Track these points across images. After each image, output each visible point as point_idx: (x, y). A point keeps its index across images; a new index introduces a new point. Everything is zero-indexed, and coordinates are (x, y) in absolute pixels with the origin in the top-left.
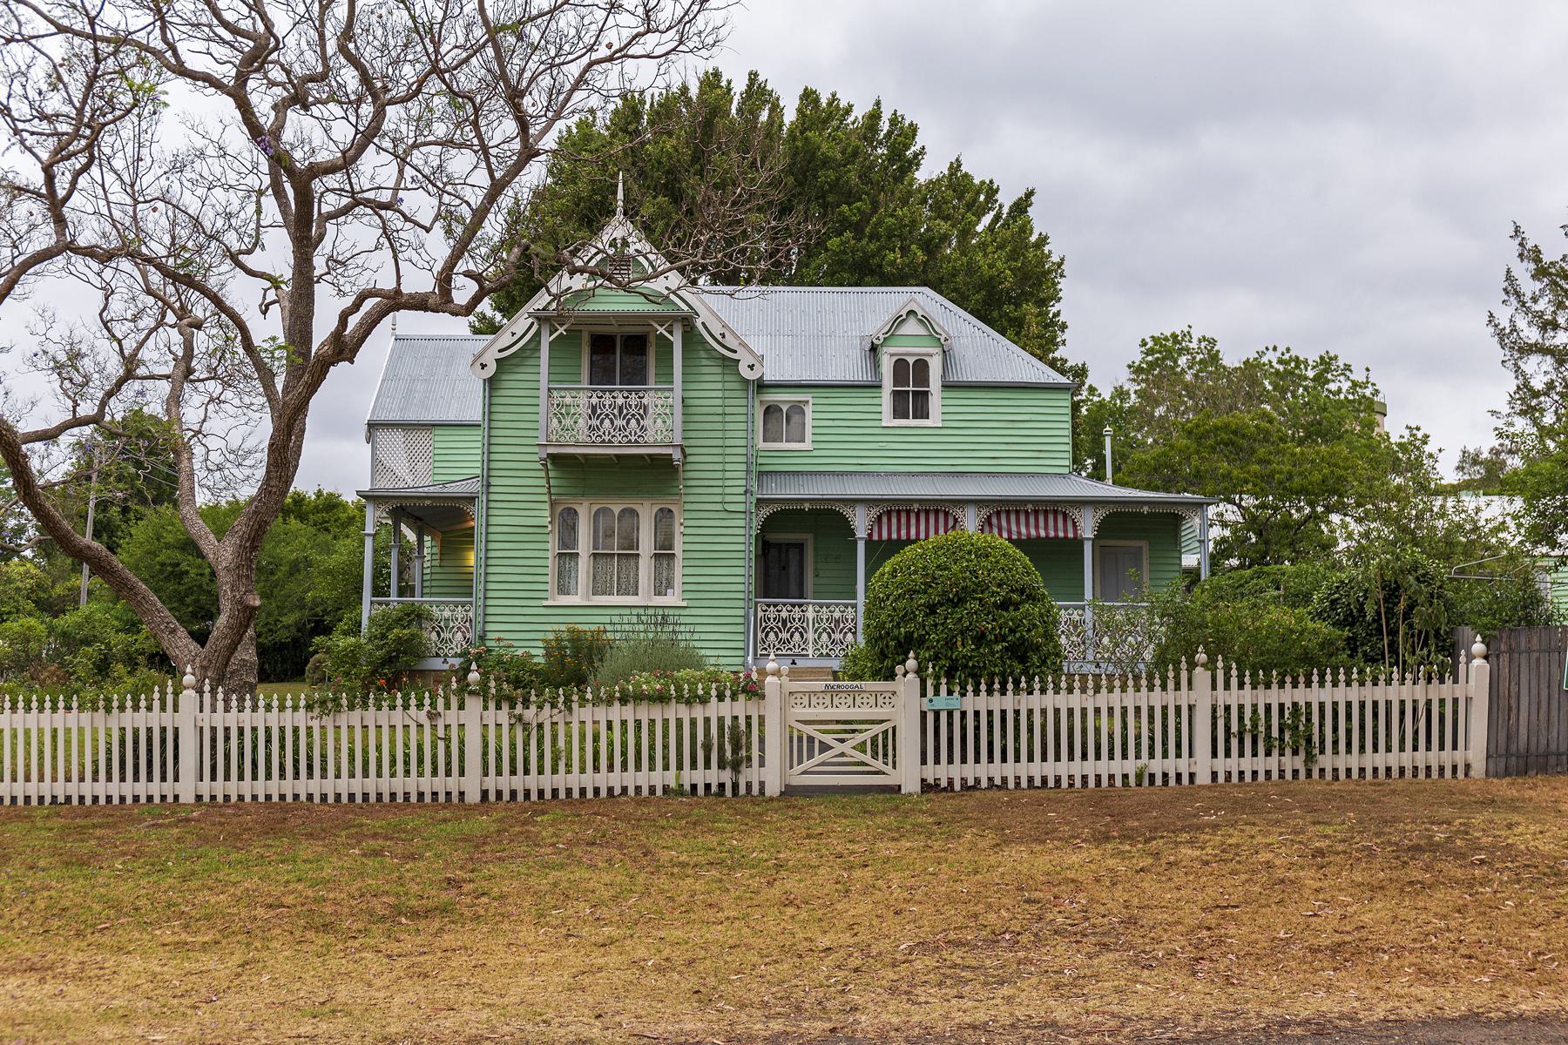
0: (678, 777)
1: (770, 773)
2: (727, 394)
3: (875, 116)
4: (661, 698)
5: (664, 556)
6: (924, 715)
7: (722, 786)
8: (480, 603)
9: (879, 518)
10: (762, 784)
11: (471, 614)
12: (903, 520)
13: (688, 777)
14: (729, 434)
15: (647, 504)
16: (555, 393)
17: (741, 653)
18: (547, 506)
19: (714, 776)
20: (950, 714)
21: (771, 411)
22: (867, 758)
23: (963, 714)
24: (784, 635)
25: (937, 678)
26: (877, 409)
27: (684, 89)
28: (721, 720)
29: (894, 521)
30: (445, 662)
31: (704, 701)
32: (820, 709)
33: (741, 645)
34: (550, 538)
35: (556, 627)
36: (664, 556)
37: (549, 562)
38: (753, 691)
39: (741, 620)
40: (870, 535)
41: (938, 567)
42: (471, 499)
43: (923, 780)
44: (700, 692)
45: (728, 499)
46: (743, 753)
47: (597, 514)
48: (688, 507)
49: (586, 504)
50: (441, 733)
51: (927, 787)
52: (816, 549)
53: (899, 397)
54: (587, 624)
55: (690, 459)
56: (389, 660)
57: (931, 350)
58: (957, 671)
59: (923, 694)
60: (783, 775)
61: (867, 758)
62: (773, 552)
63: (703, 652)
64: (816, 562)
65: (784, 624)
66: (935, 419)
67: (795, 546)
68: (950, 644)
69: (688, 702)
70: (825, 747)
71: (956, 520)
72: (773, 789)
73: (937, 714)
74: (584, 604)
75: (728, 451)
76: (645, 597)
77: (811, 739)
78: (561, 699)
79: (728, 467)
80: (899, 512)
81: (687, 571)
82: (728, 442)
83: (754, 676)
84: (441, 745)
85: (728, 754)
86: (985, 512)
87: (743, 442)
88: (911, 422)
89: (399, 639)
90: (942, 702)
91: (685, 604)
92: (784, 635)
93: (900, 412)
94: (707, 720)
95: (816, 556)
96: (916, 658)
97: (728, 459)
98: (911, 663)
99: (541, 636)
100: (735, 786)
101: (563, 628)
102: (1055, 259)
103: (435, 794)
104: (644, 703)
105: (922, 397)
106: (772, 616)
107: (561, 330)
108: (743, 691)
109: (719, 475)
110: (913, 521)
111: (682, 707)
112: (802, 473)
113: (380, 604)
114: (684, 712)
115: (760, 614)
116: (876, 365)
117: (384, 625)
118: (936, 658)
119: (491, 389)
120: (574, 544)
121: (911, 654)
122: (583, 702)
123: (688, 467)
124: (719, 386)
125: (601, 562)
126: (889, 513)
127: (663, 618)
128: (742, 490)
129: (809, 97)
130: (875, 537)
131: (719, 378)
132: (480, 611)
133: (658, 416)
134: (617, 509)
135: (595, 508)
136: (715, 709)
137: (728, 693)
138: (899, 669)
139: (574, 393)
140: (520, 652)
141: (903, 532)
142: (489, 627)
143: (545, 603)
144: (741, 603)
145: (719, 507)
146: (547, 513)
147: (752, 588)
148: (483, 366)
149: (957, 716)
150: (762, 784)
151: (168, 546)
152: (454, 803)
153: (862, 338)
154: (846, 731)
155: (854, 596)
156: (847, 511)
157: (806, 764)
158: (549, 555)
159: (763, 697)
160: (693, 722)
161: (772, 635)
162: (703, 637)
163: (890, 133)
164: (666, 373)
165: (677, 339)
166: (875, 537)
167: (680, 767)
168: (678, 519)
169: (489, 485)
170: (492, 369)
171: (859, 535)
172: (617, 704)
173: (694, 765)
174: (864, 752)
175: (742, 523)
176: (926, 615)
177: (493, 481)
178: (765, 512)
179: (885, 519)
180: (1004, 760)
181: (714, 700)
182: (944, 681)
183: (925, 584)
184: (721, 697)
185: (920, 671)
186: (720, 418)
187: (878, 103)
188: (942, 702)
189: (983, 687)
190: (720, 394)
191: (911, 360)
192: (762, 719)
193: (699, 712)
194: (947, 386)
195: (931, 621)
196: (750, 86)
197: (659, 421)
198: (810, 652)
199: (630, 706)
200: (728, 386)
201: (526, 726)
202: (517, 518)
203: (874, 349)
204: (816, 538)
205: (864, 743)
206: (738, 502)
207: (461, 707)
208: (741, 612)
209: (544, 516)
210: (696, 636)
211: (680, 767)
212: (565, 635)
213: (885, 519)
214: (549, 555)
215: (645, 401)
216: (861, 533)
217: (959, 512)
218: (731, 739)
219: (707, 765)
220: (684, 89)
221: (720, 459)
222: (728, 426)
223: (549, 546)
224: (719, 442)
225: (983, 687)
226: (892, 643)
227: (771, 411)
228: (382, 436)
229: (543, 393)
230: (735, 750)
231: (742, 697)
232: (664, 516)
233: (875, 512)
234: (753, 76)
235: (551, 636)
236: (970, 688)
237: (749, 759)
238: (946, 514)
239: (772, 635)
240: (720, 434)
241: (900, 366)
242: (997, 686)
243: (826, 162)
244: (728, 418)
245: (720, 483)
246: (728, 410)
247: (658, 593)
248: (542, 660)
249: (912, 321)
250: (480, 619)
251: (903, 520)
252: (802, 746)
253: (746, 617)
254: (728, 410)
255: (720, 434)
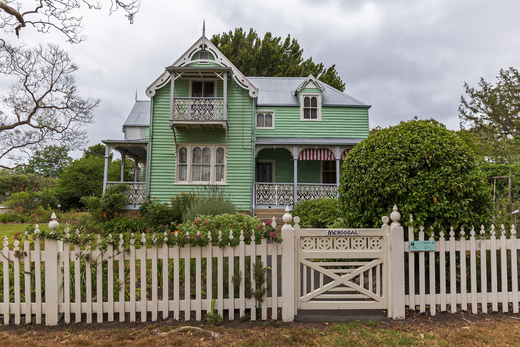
0: (213, 304)
1: (287, 302)
2: (244, 104)
3: (288, 40)
4: (201, 243)
5: (220, 165)
6: (406, 255)
7: (248, 311)
8: (148, 184)
9: (302, 152)
10: (280, 309)
11: (145, 188)
12: (311, 153)
13: (222, 304)
14: (245, 119)
15: (213, 146)
16: (176, 100)
17: (250, 203)
18: (175, 146)
19: (242, 303)
20: (427, 254)
21: (260, 115)
22: (360, 288)
23: (437, 254)
24: (266, 197)
25: (417, 226)
26: (298, 115)
27: (231, 33)
28: (248, 260)
29: (308, 153)
30: (135, 207)
31: (235, 244)
32: (324, 251)
33: (249, 200)
34: (176, 159)
35: (176, 193)
36: (220, 165)
37: (175, 168)
38: (273, 236)
39: (249, 191)
40: (299, 158)
41: (412, 142)
42: (146, 144)
43: (407, 306)
44: (231, 237)
45: (245, 144)
46: (265, 285)
47: (194, 150)
48: (229, 147)
49: (190, 146)
50: (27, 269)
51: (409, 312)
52: (276, 165)
53: (306, 111)
54: (187, 191)
55: (230, 129)
56: (112, 206)
57: (318, 94)
58: (437, 222)
59: (406, 239)
60: (296, 301)
61: (360, 288)
62: (261, 167)
63: (235, 203)
64: (276, 170)
65: (266, 192)
66: (319, 118)
67: (270, 162)
68: (430, 202)
69: (222, 245)
70: (328, 280)
71: (332, 153)
72: (288, 315)
73: (417, 255)
74: (189, 183)
75: (245, 126)
76: (212, 181)
77: (317, 273)
78: (122, 242)
79: (245, 132)
80: (310, 150)
81: (229, 172)
82: (245, 122)
83: (274, 225)
84: (27, 278)
85: (253, 286)
86: (343, 150)
87: (250, 122)
88: (311, 120)
89: (114, 198)
90: (421, 245)
91: (228, 184)
92: (266, 197)
93: (306, 116)
94: (237, 259)
95: (276, 168)
96: (399, 211)
97: (245, 129)
98: (395, 215)
99: (171, 196)
100: (259, 311)
101: (179, 193)
102: (343, 83)
103: (23, 315)
104: (187, 246)
105: (314, 111)
106: (261, 189)
107: (179, 75)
108: (265, 237)
109: (241, 135)
110: (315, 153)
111: (217, 249)
112: (271, 138)
113: (111, 184)
114: (218, 253)
115: (257, 188)
116: (298, 100)
117: (111, 191)
118: (417, 210)
119: (154, 102)
120: (185, 162)
121: (395, 207)
122: (139, 244)
123: (229, 132)
124: (241, 101)
125: (196, 168)
126: (306, 150)
127: (216, 188)
128: (250, 141)
129: (268, 35)
130: (301, 159)
131: (241, 98)
132: (148, 187)
133: (218, 110)
134: (202, 148)
135: (193, 147)
136: (243, 250)
137: (253, 238)
138: (385, 219)
139: (184, 100)
140: (162, 203)
141: (311, 157)
142: (152, 193)
143: (174, 184)
144: (249, 184)
145: (241, 147)
146: (175, 149)
147: (254, 178)
148: (150, 92)
149: (432, 256)
150: (280, 309)
151: (75, 171)
152: (35, 326)
153: (291, 92)
154: (343, 267)
155: (293, 182)
156: (290, 149)
157: (314, 293)
158: (176, 165)
159: (280, 241)
160: (226, 260)
161: (261, 196)
162: (234, 197)
163: (292, 45)
164: (221, 94)
165: (225, 79)
166: (301, 159)
167: (215, 296)
168: (225, 151)
169: (152, 138)
170: (154, 93)
171: (294, 158)
172: (165, 246)
173: (226, 295)
174: (358, 283)
175: (250, 153)
176: (409, 177)
177: (154, 137)
178: (259, 149)
179: (304, 152)
180: (459, 290)
181: (242, 243)
182: (422, 228)
183: (405, 153)
184: (247, 241)
185: (402, 222)
186: (242, 113)
187: (289, 35)
188: (421, 245)
189: (452, 233)
190: (241, 104)
191: (310, 97)
192: (279, 258)
193: (230, 253)
194: (324, 107)
195: (413, 181)
196: (250, 33)
197: (218, 111)
198: (276, 203)
199: (176, 248)
200: (245, 101)
201: (94, 266)
202: (164, 150)
203: (296, 95)
204: (276, 161)
205: (358, 276)
206: (249, 145)
207: (42, 248)
208: (250, 188)
209: (173, 150)
210: (231, 197)
211: (215, 296)
212: (180, 197)
213: (304, 152)
214: (176, 165)
215: (212, 103)
216: (296, 157)
217: (333, 150)
218: (256, 275)
219: (237, 295)
220: (231, 33)
221: (241, 129)
222: (245, 116)
223: (175, 162)
224: (241, 122)
225: (452, 233)
226: (376, 199)
227: (260, 115)
228: (128, 130)
229: (172, 100)
230: (258, 285)
231: (264, 241)
232: (220, 151)
233: (301, 149)
234: (251, 30)
235: (175, 197)
236: (442, 234)
237: (269, 288)
238: (328, 150)
239: (261, 196)
240: (241, 119)
241: (306, 99)
242: (463, 232)
243: (273, 52)
244: (245, 113)
245: (241, 138)
246: (245, 110)
247: (218, 180)
248: (170, 206)
249: (311, 83)
250: (148, 190)
251: (311, 153)
252: (310, 279)
253: (251, 189)
254: (245, 110)
255: (241, 119)
